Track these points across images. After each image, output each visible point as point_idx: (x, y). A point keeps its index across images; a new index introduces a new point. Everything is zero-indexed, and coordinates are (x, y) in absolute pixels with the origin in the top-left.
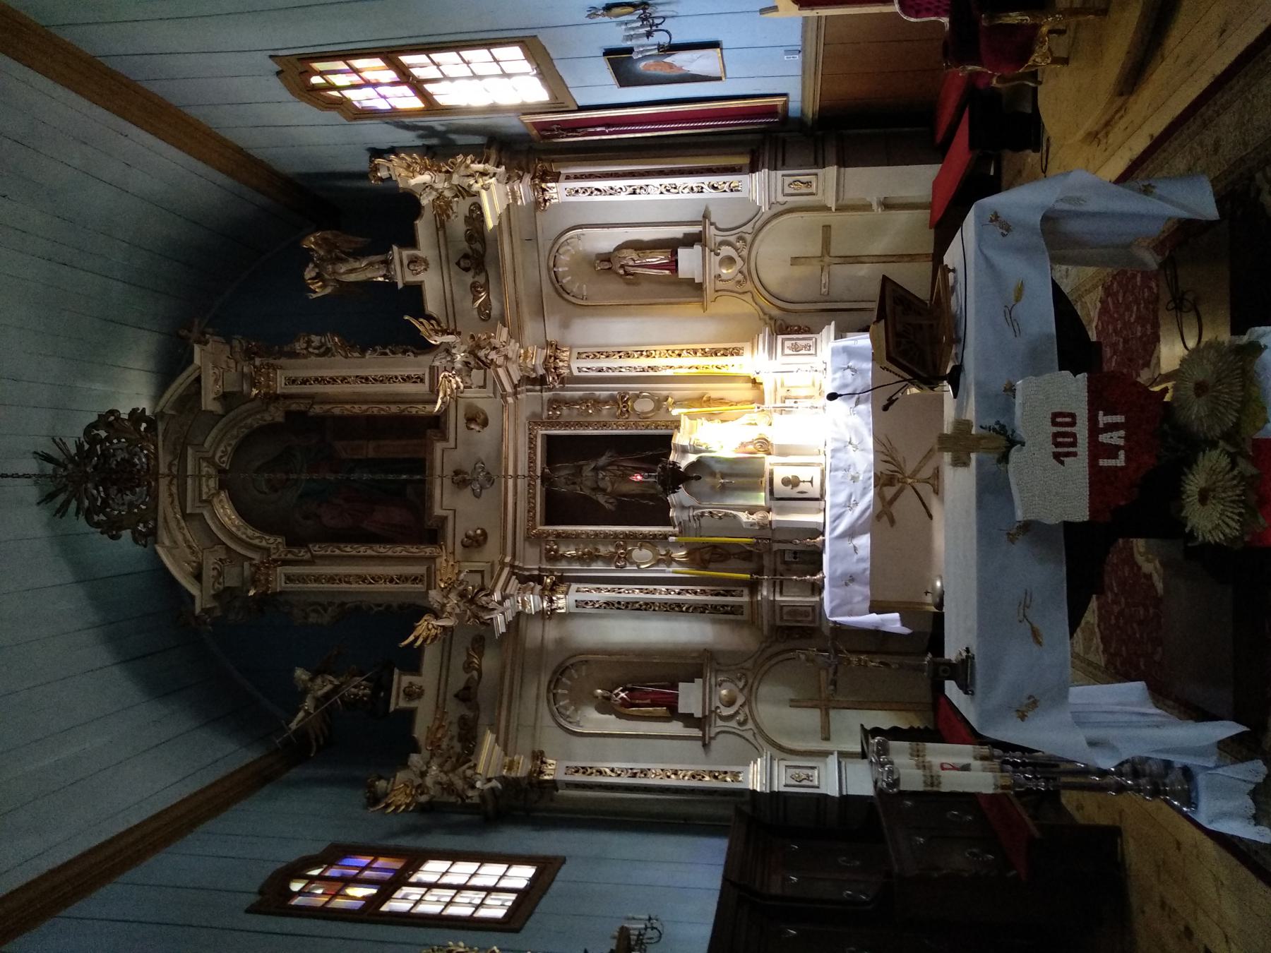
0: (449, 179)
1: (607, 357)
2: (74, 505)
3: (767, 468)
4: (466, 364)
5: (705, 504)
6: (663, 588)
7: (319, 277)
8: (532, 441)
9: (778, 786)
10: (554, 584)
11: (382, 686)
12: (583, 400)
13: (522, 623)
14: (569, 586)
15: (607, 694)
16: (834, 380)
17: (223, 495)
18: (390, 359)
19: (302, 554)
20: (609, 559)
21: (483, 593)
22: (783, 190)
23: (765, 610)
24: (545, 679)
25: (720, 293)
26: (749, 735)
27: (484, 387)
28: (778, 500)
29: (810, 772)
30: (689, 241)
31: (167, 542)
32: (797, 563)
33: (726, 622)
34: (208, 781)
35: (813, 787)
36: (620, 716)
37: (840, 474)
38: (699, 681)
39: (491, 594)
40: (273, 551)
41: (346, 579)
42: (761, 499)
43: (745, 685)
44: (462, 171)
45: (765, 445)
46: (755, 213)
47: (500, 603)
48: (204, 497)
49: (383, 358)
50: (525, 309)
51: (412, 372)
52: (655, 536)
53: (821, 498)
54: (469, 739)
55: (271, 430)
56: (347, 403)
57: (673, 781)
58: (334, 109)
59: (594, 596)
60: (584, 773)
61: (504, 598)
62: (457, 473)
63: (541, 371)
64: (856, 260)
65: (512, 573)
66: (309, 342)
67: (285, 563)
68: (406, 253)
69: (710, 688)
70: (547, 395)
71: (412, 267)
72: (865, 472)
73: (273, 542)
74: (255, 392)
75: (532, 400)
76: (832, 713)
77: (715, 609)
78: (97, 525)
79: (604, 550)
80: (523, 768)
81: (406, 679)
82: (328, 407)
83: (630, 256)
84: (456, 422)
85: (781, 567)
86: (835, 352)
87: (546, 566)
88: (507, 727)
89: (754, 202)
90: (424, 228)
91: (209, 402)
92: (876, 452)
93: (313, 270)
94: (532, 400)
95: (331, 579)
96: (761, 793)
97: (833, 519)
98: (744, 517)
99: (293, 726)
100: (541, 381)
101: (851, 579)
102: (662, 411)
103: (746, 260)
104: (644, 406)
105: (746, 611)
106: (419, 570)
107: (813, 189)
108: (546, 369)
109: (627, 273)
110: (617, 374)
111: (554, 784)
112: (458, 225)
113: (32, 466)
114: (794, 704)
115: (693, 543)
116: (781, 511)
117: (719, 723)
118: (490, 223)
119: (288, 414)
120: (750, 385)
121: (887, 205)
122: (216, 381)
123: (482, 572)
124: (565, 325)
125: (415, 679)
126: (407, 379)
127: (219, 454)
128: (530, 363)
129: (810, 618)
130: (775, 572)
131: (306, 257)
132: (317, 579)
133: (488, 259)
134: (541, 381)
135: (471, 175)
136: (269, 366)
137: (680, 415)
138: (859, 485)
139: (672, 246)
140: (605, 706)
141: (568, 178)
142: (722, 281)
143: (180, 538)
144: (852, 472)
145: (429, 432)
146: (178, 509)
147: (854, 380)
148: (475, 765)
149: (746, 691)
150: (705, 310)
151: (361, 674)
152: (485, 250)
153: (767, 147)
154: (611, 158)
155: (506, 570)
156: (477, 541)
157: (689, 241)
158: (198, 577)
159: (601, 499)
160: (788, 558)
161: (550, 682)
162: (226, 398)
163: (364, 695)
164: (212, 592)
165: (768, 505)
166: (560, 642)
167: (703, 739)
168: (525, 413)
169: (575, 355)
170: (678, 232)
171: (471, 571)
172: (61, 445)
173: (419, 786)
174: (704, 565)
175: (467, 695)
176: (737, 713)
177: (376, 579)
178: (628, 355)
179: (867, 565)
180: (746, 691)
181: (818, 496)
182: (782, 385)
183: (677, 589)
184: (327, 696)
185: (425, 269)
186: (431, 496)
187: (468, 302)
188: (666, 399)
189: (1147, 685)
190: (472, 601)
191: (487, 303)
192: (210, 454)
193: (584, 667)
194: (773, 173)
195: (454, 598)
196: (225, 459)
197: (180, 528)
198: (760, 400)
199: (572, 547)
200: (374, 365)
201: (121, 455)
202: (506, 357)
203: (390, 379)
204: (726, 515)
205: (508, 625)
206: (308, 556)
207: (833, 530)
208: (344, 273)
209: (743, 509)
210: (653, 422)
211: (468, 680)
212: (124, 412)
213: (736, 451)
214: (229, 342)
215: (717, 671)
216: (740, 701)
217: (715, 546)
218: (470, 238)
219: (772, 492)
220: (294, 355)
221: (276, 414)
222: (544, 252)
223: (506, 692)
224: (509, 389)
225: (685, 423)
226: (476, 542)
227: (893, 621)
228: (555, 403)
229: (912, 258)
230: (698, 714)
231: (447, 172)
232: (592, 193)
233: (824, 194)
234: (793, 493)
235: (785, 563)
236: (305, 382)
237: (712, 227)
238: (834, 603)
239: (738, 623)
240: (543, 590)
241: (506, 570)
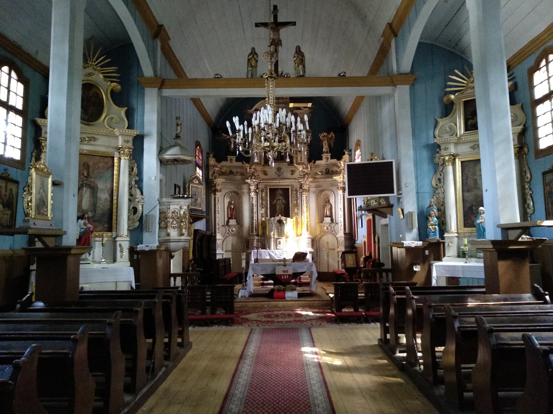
5: (275, 225)
6: (256, 216)
8: (288, 185)
9: (217, 241)
20: (262, 203)
24: (235, 190)
26: (225, 235)
30: (332, 220)
37: (282, 252)
38: (236, 224)
42: (276, 237)
45: (287, 237)
52: (267, 214)
53: (277, 249)
59: (254, 201)
63: (303, 188)
64: (328, 256)
65: (258, 182)
68: (329, 157)
70: (298, 189)
75: (297, 185)
76: (231, 252)
77: (252, 227)
83: (329, 207)
90: (334, 161)
94: (297, 185)
98: (272, 233)
100: (301, 188)
102: (295, 215)
104: (296, 210)
110: (303, 205)
114: (232, 244)
116: (274, 241)
117: (228, 229)
124: (314, 192)
138: (279, 256)
139: (331, 216)
140: (230, 203)
157: (332, 220)
159: (275, 201)
160: (264, 243)
166: (243, 193)
167: (224, 225)
168: (294, 184)
170: (334, 217)
174: (262, 224)
175: (231, 173)
176: (230, 232)
179: (263, 258)
183: (256, 219)
188: (298, 215)
190: (253, 175)
209: (274, 233)
215: (238, 228)
216: (233, 233)
218: (332, 171)
219: (277, 239)
224: (299, 181)
228: (296, 191)
234: (278, 243)
235: (263, 242)
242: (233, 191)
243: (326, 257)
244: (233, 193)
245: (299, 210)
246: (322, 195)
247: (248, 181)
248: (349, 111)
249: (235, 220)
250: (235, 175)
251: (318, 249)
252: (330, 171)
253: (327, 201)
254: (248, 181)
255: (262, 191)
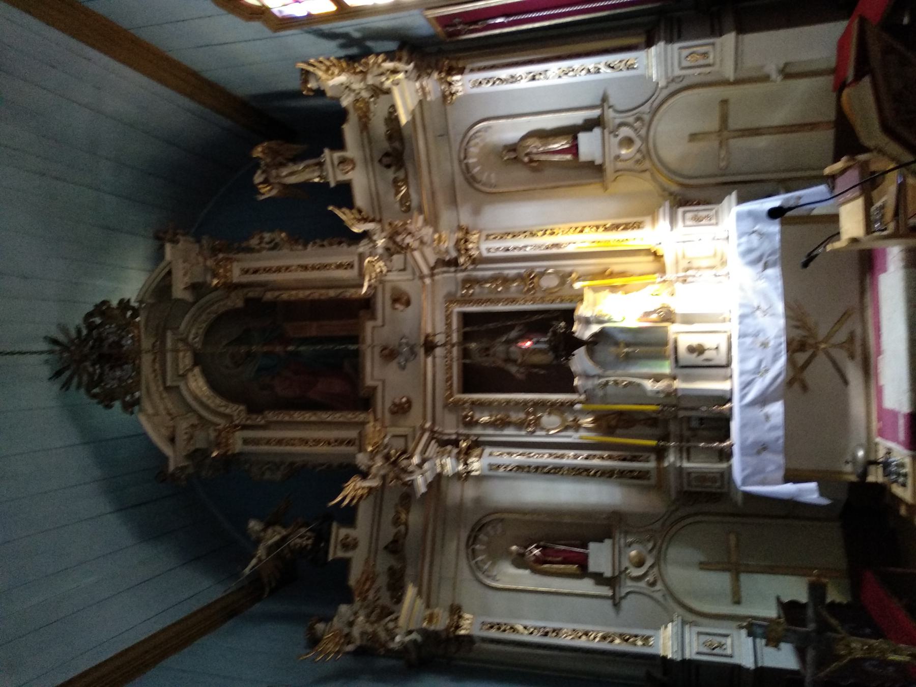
0: (364, 79)
1: (514, 236)
2: (75, 381)
3: (671, 336)
4: (387, 249)
5: (609, 372)
6: (572, 453)
7: (266, 182)
8: (448, 317)
9: (691, 653)
10: (469, 448)
11: (322, 537)
12: (493, 279)
13: (443, 482)
14: (483, 450)
15: (522, 551)
16: (739, 245)
17: (197, 370)
18: (327, 250)
19: (258, 420)
20: (520, 425)
21: (405, 456)
22: (680, 63)
23: (672, 479)
24: (464, 535)
25: (620, 173)
26: (658, 596)
27: (404, 270)
28: (683, 368)
29: (723, 640)
30: (589, 125)
31: (150, 411)
32: (703, 429)
33: (634, 486)
34: (158, 627)
35: (726, 656)
36: (535, 571)
37: (748, 340)
38: (608, 542)
39: (410, 457)
40: (235, 418)
41: (290, 442)
42: (666, 368)
43: (653, 549)
44: (376, 71)
45: (668, 316)
46: (650, 94)
47: (420, 466)
48: (181, 372)
49: (321, 250)
50: (441, 198)
51: (345, 260)
52: (562, 404)
53: (728, 365)
54: (397, 591)
55: (231, 315)
56: (293, 289)
57: (583, 642)
58: (259, 19)
59: (505, 459)
60: (499, 629)
61: (424, 461)
62: (384, 348)
63: (454, 254)
64: (755, 132)
65: (431, 438)
66: (262, 238)
67: (245, 427)
68: (337, 155)
69: (620, 551)
70: (461, 275)
71: (341, 167)
72: (776, 337)
73: (237, 411)
74: (215, 282)
75: (448, 280)
76: (744, 577)
77: (622, 474)
78: (94, 396)
79: (516, 416)
80: (442, 622)
81: (343, 532)
82: (277, 293)
83: (534, 146)
84: (383, 303)
85: (687, 433)
86: (740, 217)
87: (463, 431)
88: (430, 580)
89: (651, 78)
90: (350, 131)
91: (179, 291)
92: (787, 317)
93: (260, 176)
94: (448, 280)
95: (280, 442)
96: (671, 660)
97: (743, 386)
98: (649, 385)
99: (247, 571)
100: (454, 263)
101: (763, 448)
102: (567, 286)
103: (645, 140)
104: (550, 282)
105: (654, 474)
106: (352, 434)
107: (710, 60)
108: (459, 250)
109: (531, 161)
110: (522, 253)
111: (469, 639)
112: (379, 127)
113: (45, 346)
114: (704, 566)
115: (599, 411)
116: (687, 379)
117: (629, 583)
118: (404, 119)
119: (248, 301)
120: (651, 258)
121: (788, 73)
122: (185, 275)
123: (405, 436)
124: (477, 212)
125: (352, 533)
126: (339, 266)
127: (191, 336)
128: (444, 246)
129: (718, 484)
130: (681, 438)
131: (255, 165)
132: (268, 442)
133: (405, 157)
134: (454, 263)
135: (382, 74)
136: (227, 259)
137: (582, 289)
138: (769, 352)
139: (571, 132)
140: (520, 561)
141: (472, 71)
142: (620, 161)
143: (161, 407)
144: (761, 338)
145: (362, 313)
146: (160, 382)
147: (762, 244)
148: (397, 619)
149: (655, 552)
150: (606, 189)
151: (306, 524)
152: (404, 148)
153: (662, 27)
154: (515, 51)
155: (426, 436)
156: (403, 408)
157: (589, 125)
158: (172, 440)
159: (513, 369)
160: (694, 424)
161: (469, 537)
162: (196, 288)
163: (307, 545)
164: (184, 454)
165: (673, 373)
166: (478, 501)
167: (613, 597)
168: (442, 292)
169: (483, 237)
170: (577, 118)
171: (394, 436)
172: (64, 329)
173: (347, 635)
174: (610, 430)
175: (395, 547)
176: (645, 575)
177: (317, 442)
178: (533, 234)
179: (780, 433)
180: (655, 552)
181: (724, 362)
182: (684, 257)
183: (585, 453)
184: (278, 544)
185: (353, 169)
186: (363, 368)
187: (391, 197)
188: (570, 274)
189: (570, 369)
190: (395, 463)
191: (407, 196)
192: (184, 335)
193: (500, 525)
194: (669, 46)
195: (379, 462)
196: (197, 339)
197: (162, 398)
198: (662, 270)
199: (486, 413)
200: (312, 255)
201: (112, 338)
202: (422, 242)
203: (325, 267)
204: (630, 383)
205: (430, 486)
206: (263, 422)
207: (743, 397)
208: (287, 176)
209: (648, 377)
210: (559, 297)
211: (396, 534)
212: (115, 303)
213: (641, 320)
214: (198, 241)
215: (626, 533)
216: (649, 563)
217: (621, 413)
218: (390, 138)
219: (676, 360)
220: (250, 250)
221: (236, 301)
222: (456, 146)
223: (428, 551)
224: (426, 271)
225: (588, 296)
226: (401, 409)
227: (810, 491)
228: (470, 282)
229: (812, 126)
230: (608, 573)
231: (361, 72)
232: (494, 83)
233: (721, 64)
234: (699, 360)
235: (690, 429)
236: (256, 271)
237: (611, 110)
238: (746, 472)
239: (648, 488)
240: (459, 453)
241: (426, 436)
242: (467, 546)
243: (761, 142)
244: (478, 547)
245: (548, 268)
246: (484, 178)
247: (421, 482)
248: (200, 102)
249: (593, 546)
250: (407, 529)
251: (724, 179)
252: (389, 150)
253: (513, 155)
254: (421, 482)
255: (473, 423)
